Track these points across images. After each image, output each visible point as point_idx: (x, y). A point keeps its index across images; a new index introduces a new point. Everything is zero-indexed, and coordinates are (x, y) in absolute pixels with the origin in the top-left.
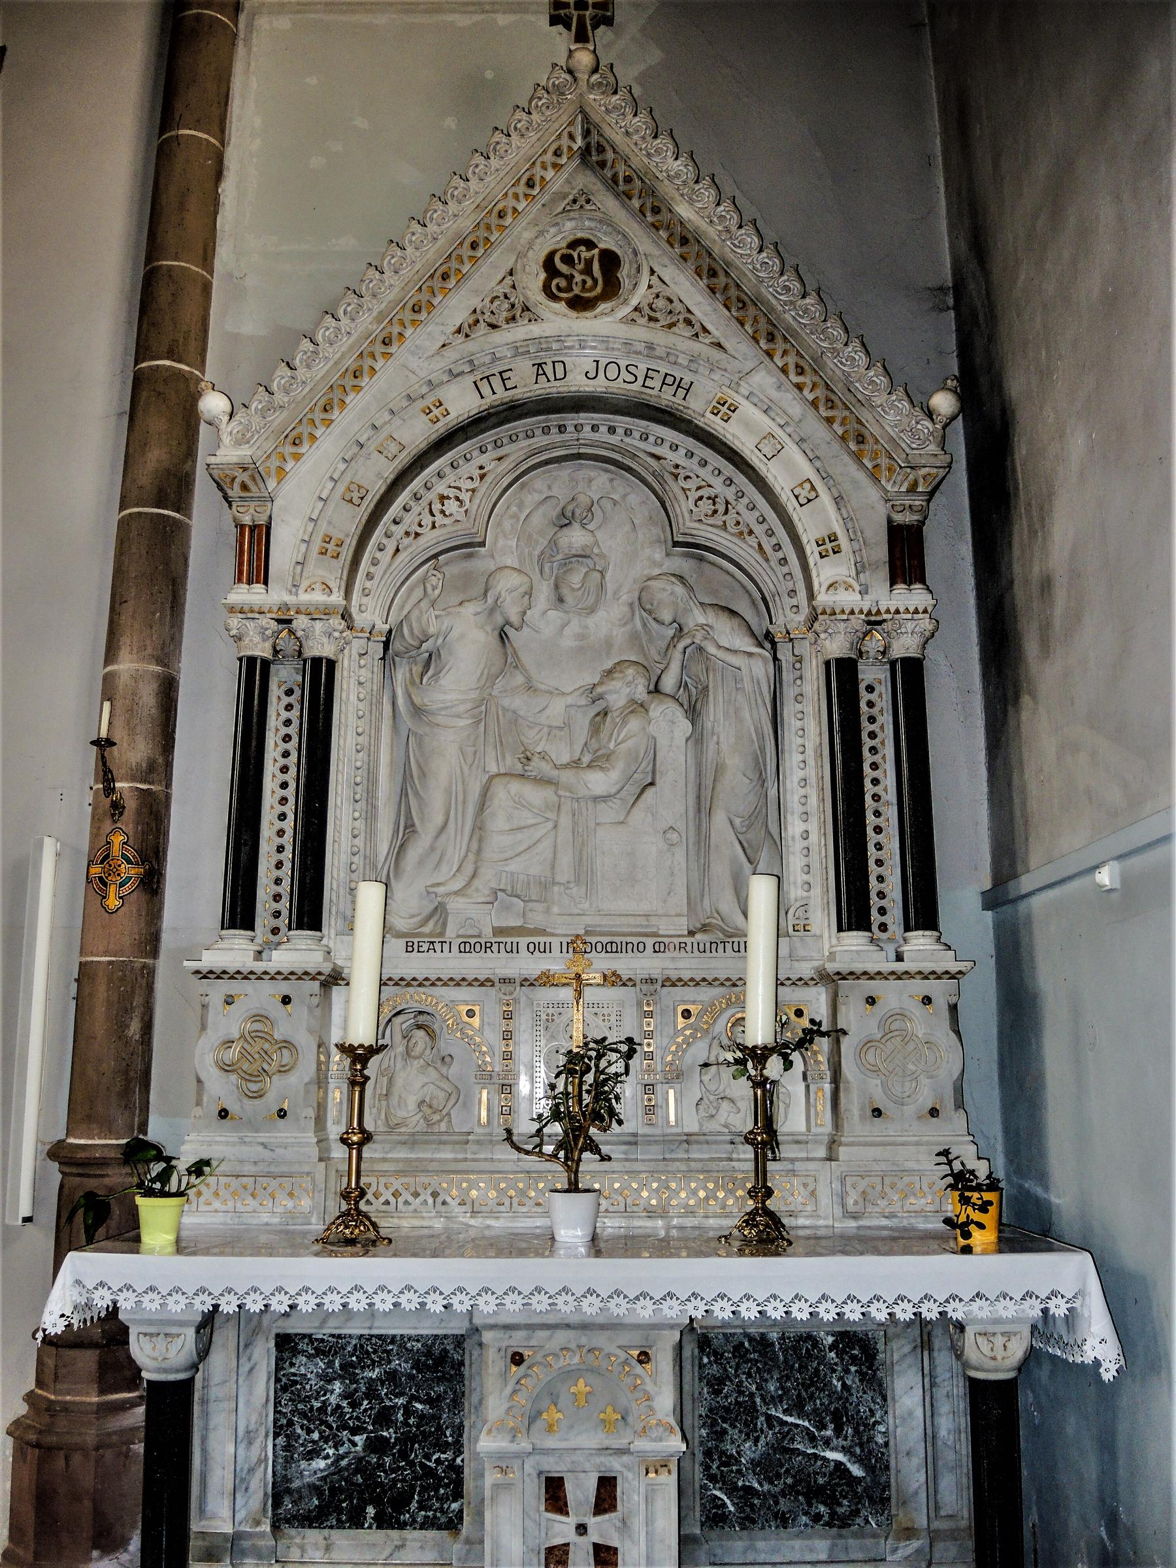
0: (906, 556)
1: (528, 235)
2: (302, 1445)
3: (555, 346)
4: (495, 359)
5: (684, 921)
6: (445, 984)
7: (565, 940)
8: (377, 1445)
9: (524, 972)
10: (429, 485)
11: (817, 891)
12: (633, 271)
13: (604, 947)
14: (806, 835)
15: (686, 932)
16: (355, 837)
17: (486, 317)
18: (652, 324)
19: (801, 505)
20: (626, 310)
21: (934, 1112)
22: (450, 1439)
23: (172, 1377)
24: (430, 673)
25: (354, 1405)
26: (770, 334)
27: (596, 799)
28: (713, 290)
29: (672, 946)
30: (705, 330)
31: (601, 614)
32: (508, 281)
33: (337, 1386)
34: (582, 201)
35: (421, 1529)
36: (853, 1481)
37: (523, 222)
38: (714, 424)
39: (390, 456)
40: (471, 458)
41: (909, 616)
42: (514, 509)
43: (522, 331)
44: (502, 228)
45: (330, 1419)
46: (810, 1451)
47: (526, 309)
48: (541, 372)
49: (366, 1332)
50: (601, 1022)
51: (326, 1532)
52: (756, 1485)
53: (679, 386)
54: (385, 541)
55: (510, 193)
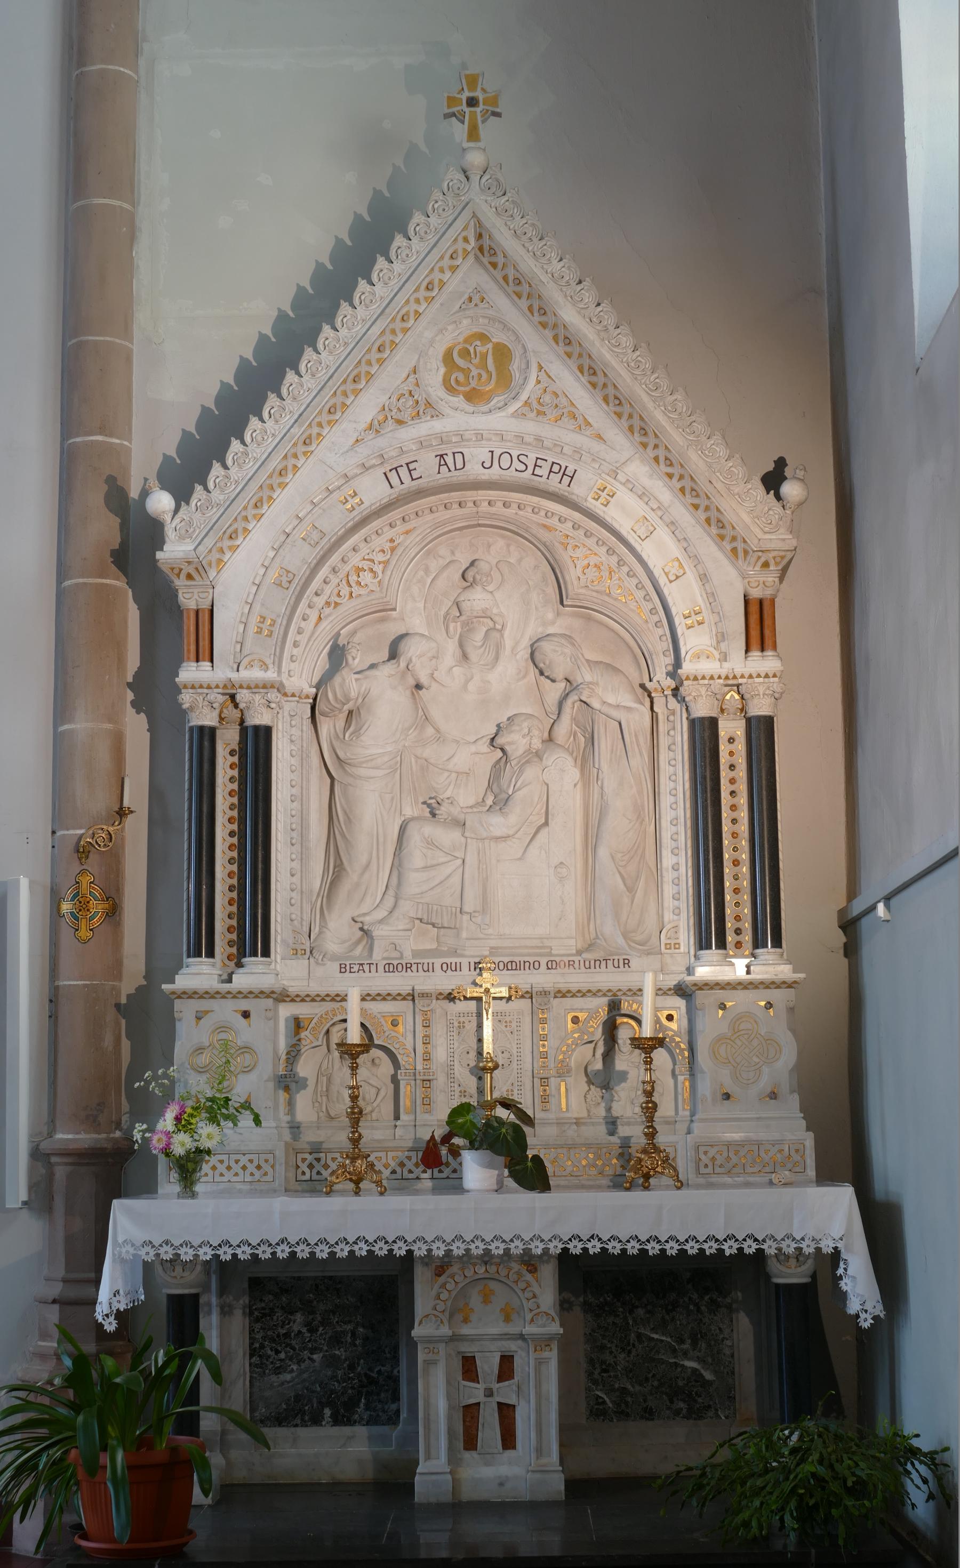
0: (759, 623)
1: (428, 334)
2: (272, 1363)
3: (454, 439)
4: (402, 451)
5: (572, 942)
6: (374, 999)
7: (473, 961)
8: (332, 1362)
9: (439, 987)
10: (346, 559)
11: (684, 915)
12: (523, 366)
13: (506, 966)
14: (675, 868)
15: (574, 952)
16: (292, 875)
17: (393, 413)
18: (540, 418)
19: (671, 582)
20: (517, 405)
21: (773, 1096)
22: (388, 1355)
23: (186, 1291)
24: (351, 729)
25: (312, 1330)
26: (642, 431)
27: (497, 839)
28: (594, 385)
29: (562, 963)
30: (588, 424)
31: (500, 668)
32: (412, 379)
33: (299, 1317)
34: (476, 299)
35: (367, 1424)
36: (706, 1384)
37: (423, 321)
38: (596, 507)
39: (312, 542)
40: (379, 536)
41: (761, 680)
42: (421, 573)
43: (426, 427)
44: (405, 331)
45: (293, 1342)
46: (672, 1361)
47: (428, 404)
48: (443, 462)
49: (320, 1274)
50: (504, 1028)
51: (293, 1429)
52: (629, 1387)
53: (564, 474)
54: (308, 611)
55: (412, 299)
